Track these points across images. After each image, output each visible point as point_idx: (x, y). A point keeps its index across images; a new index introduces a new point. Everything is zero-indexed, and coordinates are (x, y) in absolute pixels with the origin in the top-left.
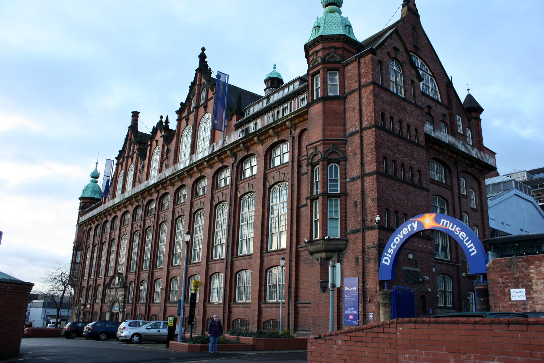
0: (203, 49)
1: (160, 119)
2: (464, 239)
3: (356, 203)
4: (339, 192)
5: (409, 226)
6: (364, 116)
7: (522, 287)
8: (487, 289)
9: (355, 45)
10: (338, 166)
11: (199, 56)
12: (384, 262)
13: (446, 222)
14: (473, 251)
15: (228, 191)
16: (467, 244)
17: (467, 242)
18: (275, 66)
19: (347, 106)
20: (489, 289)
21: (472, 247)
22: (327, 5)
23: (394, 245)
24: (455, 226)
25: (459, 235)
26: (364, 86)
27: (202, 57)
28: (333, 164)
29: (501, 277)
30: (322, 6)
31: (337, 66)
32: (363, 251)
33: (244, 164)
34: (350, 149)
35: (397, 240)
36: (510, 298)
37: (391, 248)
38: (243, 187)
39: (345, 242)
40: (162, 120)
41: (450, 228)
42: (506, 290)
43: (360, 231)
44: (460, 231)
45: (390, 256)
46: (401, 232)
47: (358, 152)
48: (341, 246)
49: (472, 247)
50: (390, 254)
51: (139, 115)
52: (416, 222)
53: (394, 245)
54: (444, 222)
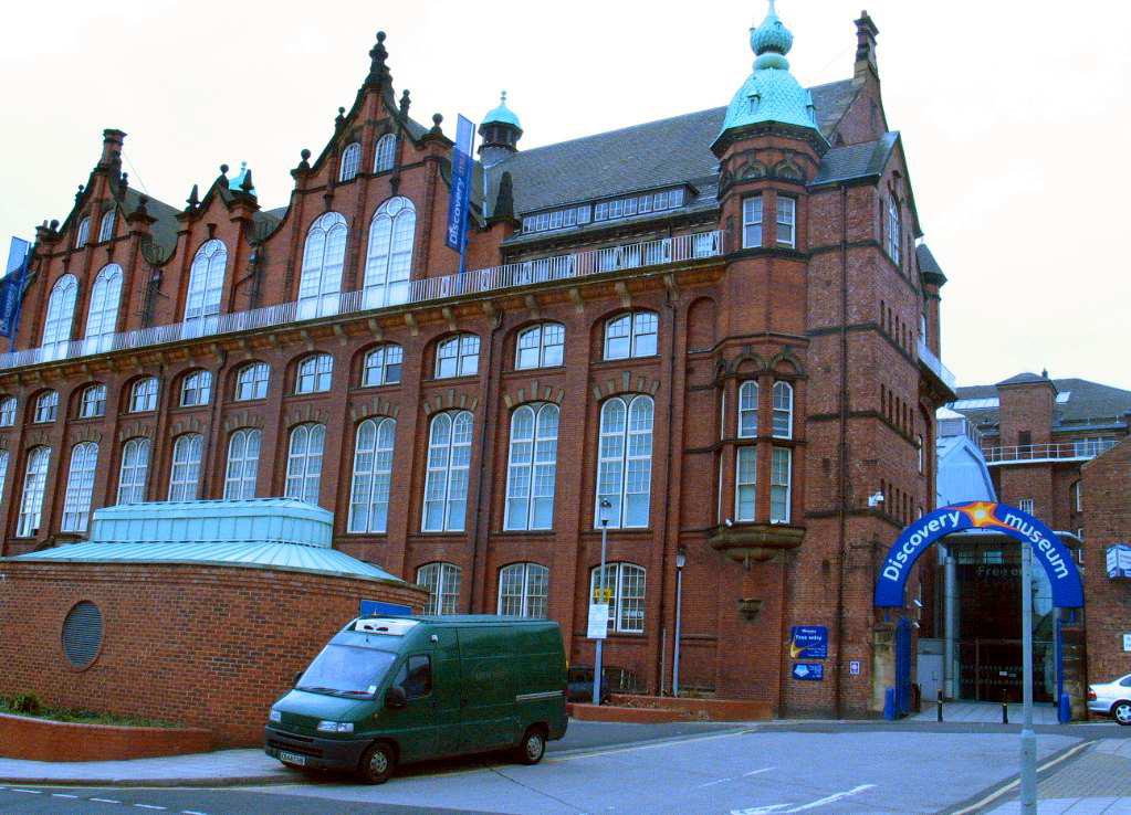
0: (381, 36)
1: (221, 173)
2: (1047, 550)
4: (790, 437)
5: (942, 519)
6: (853, 302)
8: (1085, 632)
10: (790, 387)
11: (372, 54)
12: (886, 575)
13: (1015, 519)
14: (1063, 572)
15: (152, 423)
16: (1051, 560)
18: (504, 93)
19: (812, 274)
20: (1088, 633)
21: (1060, 565)
22: (760, 51)
23: (909, 548)
24: (1032, 528)
25: (1037, 543)
26: (855, 245)
27: (379, 54)
28: (750, 382)
29: (1110, 615)
30: (749, 48)
31: (794, 188)
32: (842, 552)
33: (300, 366)
34: (817, 359)
35: (916, 540)
36: (1123, 648)
37: (903, 553)
38: (180, 424)
39: (800, 532)
40: (226, 174)
41: (1022, 531)
42: (1117, 636)
43: (835, 515)
44: (1041, 538)
45: (900, 566)
46: (925, 528)
47: (836, 367)
48: (795, 539)
50: (900, 562)
51: (125, 140)
52: (957, 514)
53: (909, 548)
54: (1011, 520)
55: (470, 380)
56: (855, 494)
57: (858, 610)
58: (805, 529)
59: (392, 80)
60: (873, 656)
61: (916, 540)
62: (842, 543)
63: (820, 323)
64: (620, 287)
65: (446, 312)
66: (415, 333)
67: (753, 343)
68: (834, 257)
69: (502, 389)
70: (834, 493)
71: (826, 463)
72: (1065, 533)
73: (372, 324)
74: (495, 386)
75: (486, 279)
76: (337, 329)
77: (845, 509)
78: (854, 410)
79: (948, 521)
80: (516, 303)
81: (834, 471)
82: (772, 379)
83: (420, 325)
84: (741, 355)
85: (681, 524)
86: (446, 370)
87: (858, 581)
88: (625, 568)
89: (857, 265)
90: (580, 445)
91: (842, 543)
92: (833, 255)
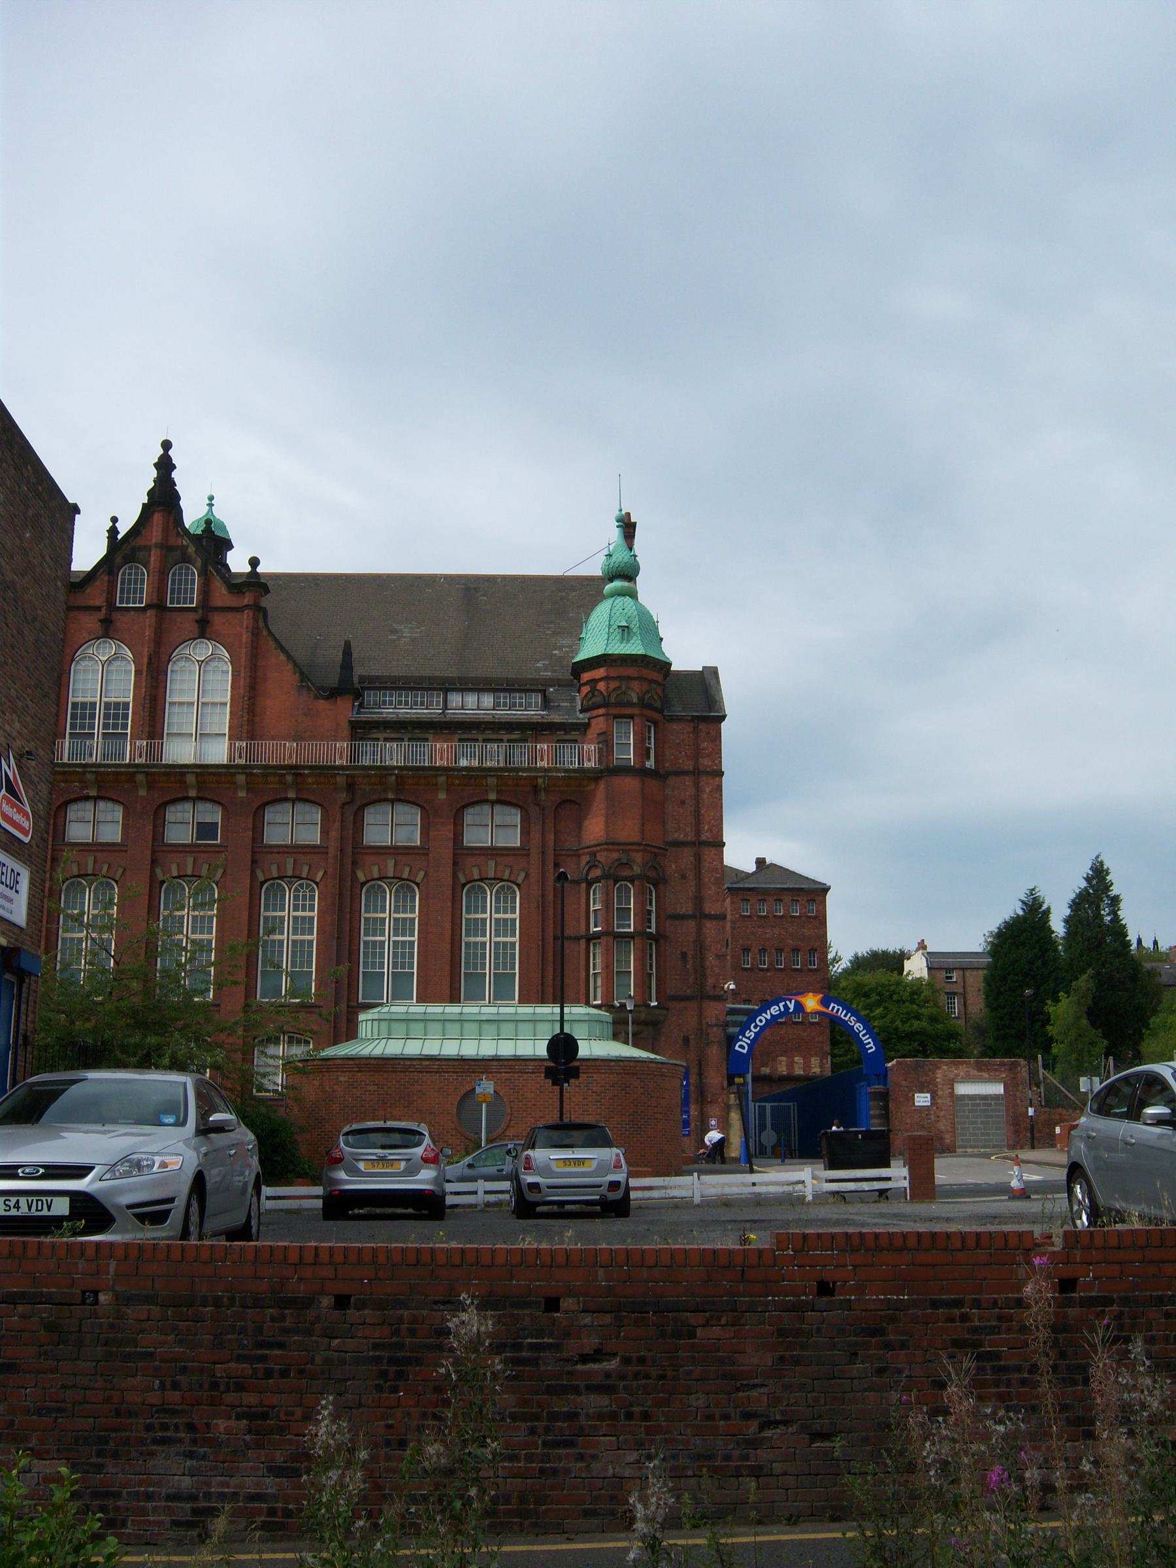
0: (167, 445)
3: (684, 955)
4: (632, 930)
5: (781, 1005)
7: (928, 1092)
8: (888, 1093)
9: (636, 661)
10: (630, 886)
11: (157, 466)
12: (737, 1048)
13: (837, 1007)
14: (871, 1048)
16: (863, 1039)
17: (864, 1035)
21: (869, 1043)
27: (165, 466)
28: (622, 883)
35: (761, 1021)
39: (665, 1012)
42: (910, 1095)
45: (749, 1042)
47: (691, 875)
49: (869, 1043)
50: (748, 1038)
53: (755, 1027)
54: (834, 1007)
55: (109, 847)
56: (710, 981)
57: (715, 1078)
58: (667, 1009)
59: (179, 498)
60: (728, 1113)
61: (761, 1021)
62: (700, 1023)
63: (676, 835)
64: (492, 781)
65: (289, 779)
66: (242, 794)
67: (629, 850)
68: (688, 781)
69: (354, 863)
70: (691, 980)
71: (684, 955)
72: (852, 1020)
73: (191, 779)
74: (348, 861)
75: (337, 752)
76: (140, 778)
77: (704, 994)
78: (707, 913)
79: (786, 1006)
80: (422, 781)
81: (690, 963)
82: (611, 882)
83: (150, 787)
84: (620, 859)
85: (349, 1000)
86: (78, 831)
87: (715, 1053)
88: (289, 1037)
89: (707, 790)
90: (448, 926)
91: (700, 1023)
92: (687, 778)
